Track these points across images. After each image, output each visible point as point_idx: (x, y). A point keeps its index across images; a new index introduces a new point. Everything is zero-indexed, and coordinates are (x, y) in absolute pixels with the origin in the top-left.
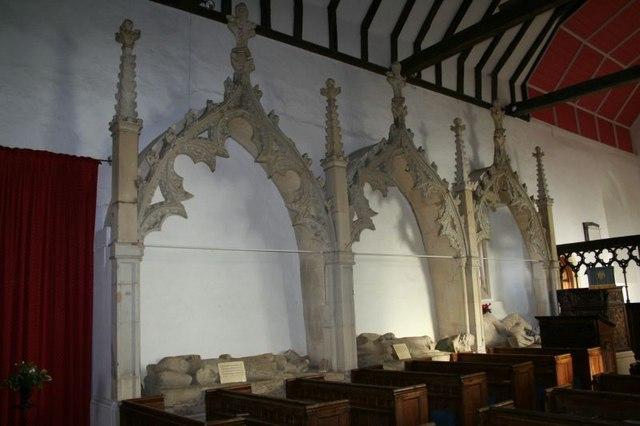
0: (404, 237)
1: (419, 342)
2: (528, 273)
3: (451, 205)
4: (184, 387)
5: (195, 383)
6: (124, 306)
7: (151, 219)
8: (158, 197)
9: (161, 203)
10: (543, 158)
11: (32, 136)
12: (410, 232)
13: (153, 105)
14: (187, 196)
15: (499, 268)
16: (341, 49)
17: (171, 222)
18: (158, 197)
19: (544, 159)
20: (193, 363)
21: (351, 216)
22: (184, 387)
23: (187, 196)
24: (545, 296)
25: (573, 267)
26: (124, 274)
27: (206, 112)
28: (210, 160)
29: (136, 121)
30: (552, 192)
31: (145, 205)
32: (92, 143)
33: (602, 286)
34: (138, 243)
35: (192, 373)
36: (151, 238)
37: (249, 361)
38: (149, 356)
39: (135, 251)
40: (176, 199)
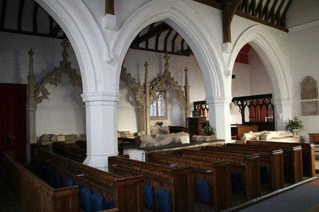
0: (128, 100)
1: (126, 133)
2: (181, 112)
3: (140, 92)
4: (47, 141)
5: (50, 140)
6: (31, 122)
7: (39, 101)
8: (41, 94)
9: (41, 96)
10: (148, 67)
11: (9, 80)
12: (131, 99)
13: (37, 69)
14: (49, 94)
15: (171, 109)
16: (23, 29)
17: (44, 101)
18: (41, 94)
19: (188, 73)
20: (51, 136)
21: (150, 98)
22: (47, 141)
23: (49, 94)
24: (185, 120)
25: (254, 106)
26: (31, 114)
27: (54, 71)
28: (54, 83)
29: (33, 76)
30: (190, 84)
31: (37, 97)
32: (25, 81)
33: (197, 117)
34: (36, 107)
35: (50, 138)
36: (39, 105)
37: (66, 136)
38: (39, 134)
39: (34, 109)
40: (46, 94)
